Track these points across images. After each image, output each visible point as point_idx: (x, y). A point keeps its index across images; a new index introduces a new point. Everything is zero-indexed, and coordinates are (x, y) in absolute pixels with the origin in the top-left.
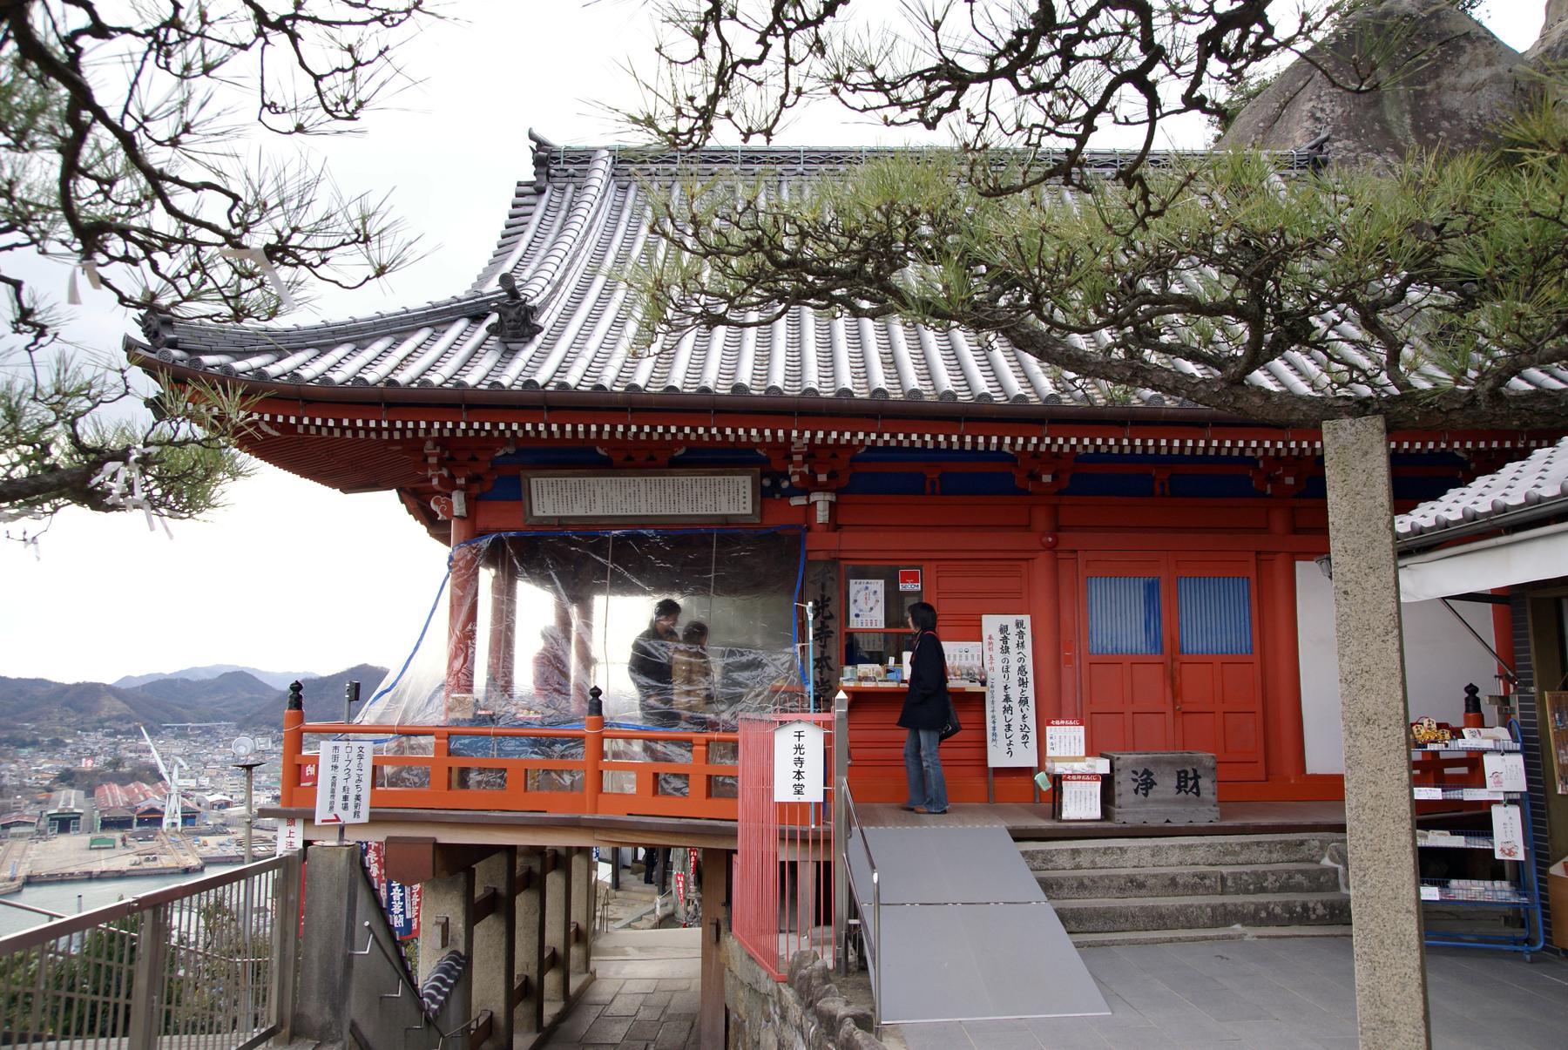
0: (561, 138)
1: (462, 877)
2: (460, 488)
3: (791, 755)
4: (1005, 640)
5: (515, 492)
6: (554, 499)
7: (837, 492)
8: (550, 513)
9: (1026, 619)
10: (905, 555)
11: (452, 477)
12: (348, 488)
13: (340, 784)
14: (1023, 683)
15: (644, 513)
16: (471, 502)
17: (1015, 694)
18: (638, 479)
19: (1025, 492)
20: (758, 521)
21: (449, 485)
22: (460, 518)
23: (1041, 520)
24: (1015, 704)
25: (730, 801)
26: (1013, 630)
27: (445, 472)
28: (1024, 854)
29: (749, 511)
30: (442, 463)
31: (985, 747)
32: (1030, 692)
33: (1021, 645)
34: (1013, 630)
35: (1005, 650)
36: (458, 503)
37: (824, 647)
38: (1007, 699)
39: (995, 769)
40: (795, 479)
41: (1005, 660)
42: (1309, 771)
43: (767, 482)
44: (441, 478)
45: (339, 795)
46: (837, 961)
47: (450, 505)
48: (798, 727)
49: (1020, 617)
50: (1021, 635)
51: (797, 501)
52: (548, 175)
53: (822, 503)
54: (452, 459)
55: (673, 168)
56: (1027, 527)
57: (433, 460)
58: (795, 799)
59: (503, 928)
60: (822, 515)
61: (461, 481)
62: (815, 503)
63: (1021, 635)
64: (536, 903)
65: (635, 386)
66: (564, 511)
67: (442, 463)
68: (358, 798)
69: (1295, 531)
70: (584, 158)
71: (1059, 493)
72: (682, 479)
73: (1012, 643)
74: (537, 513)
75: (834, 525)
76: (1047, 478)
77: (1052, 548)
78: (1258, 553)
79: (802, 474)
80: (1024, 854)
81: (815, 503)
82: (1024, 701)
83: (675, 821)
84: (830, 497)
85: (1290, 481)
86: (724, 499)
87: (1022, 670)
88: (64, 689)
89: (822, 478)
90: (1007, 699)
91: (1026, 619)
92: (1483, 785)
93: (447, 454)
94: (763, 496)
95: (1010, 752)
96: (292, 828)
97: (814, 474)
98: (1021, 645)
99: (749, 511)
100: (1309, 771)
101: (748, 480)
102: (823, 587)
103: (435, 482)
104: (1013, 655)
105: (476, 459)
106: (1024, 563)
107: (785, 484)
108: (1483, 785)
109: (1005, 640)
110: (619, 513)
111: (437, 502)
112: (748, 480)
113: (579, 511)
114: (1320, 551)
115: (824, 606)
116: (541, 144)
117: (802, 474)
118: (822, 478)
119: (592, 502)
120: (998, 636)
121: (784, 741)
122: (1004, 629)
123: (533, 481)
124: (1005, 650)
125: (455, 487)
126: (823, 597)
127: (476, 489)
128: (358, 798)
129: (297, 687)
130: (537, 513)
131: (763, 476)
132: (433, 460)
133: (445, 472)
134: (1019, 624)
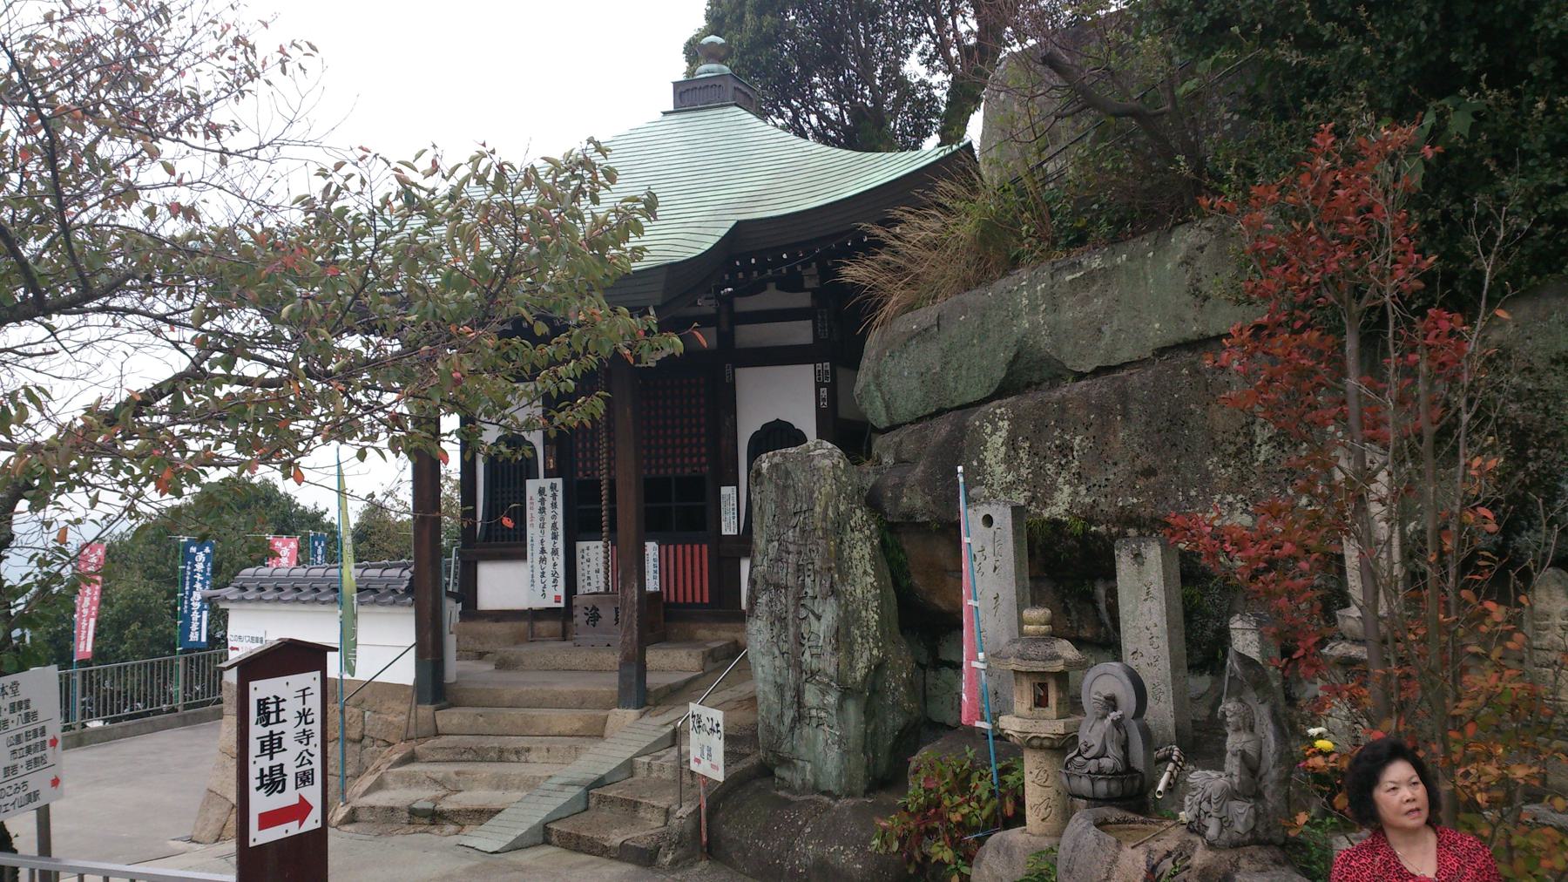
4: (542, 501)
10: (689, 566)
14: (555, 537)
26: (548, 492)
33: (554, 505)
34: (548, 492)
35: (542, 510)
38: (543, 551)
41: (542, 519)
42: (810, 322)
46: (909, 516)
49: (555, 480)
50: (554, 496)
63: (554, 496)
73: (548, 504)
82: (555, 552)
90: (543, 551)
92: (459, 658)
98: (554, 505)
100: (810, 322)
108: (459, 658)
109: (542, 501)
114: (676, 85)
122: (541, 491)
124: (542, 510)
134: (553, 487)
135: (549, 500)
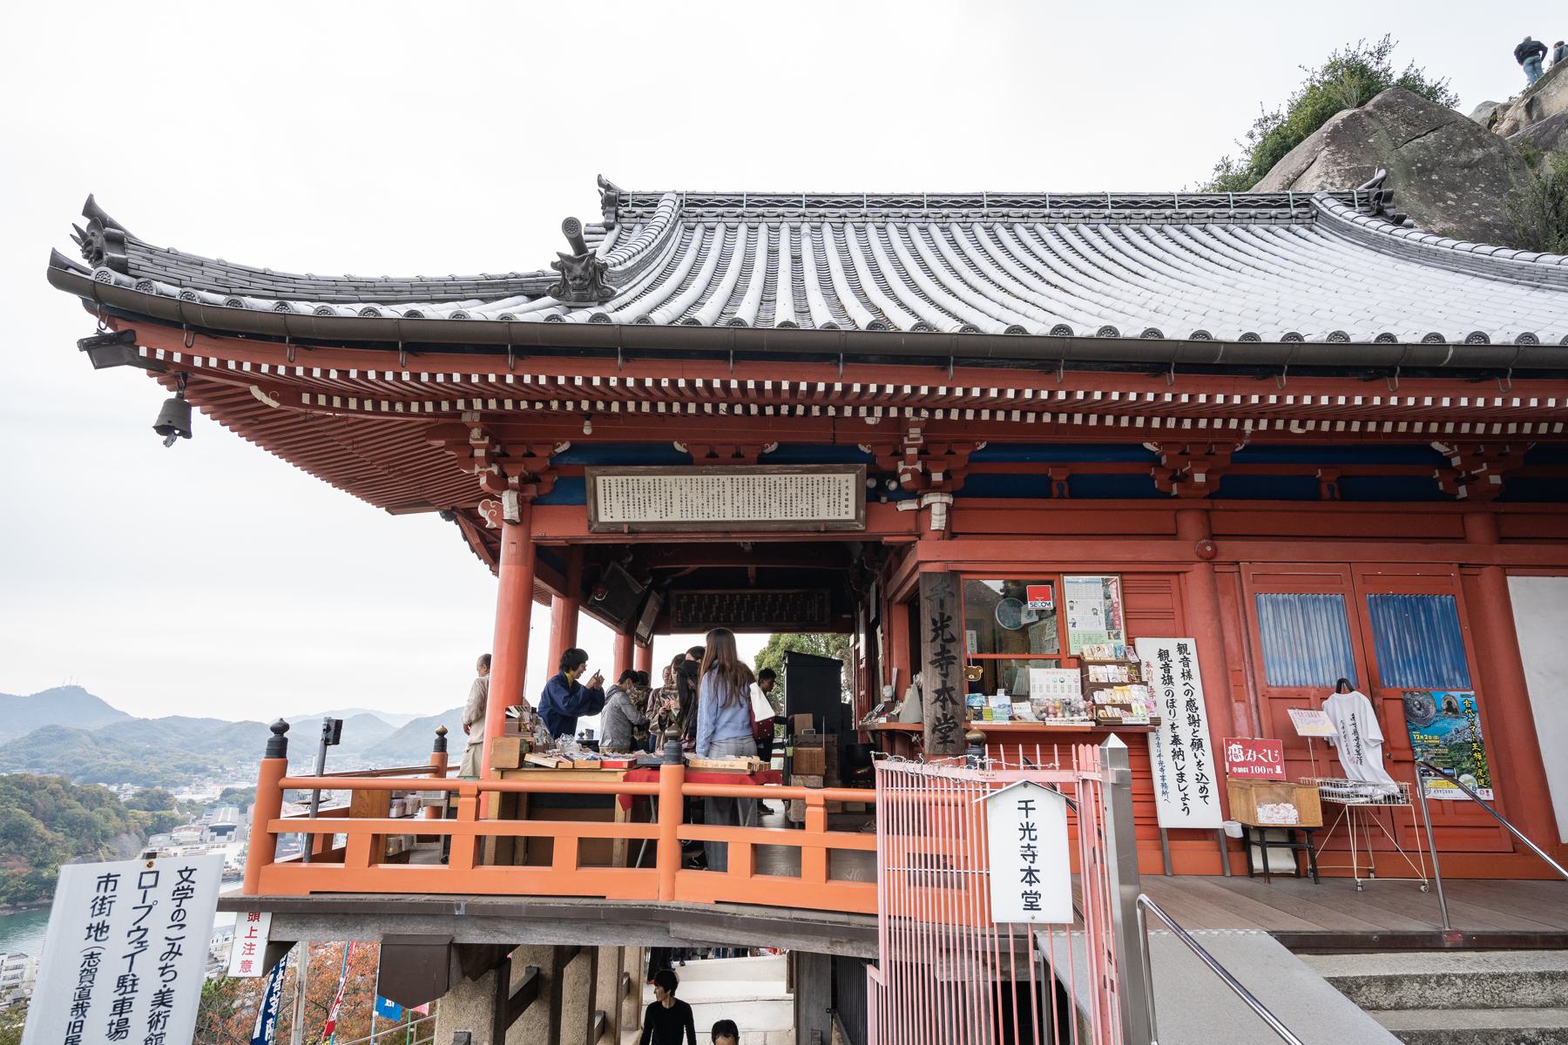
0: (627, 184)
1: (491, 977)
2: (513, 488)
3: (1015, 842)
4: (1166, 667)
5: (577, 492)
6: (628, 502)
7: (955, 494)
8: (618, 518)
9: (1190, 643)
11: (505, 476)
12: (396, 507)
13: (111, 968)
14: (1194, 721)
15: (729, 518)
16: (525, 505)
17: (1185, 733)
18: (723, 478)
19: (1167, 495)
20: (861, 527)
21: (500, 482)
22: (511, 522)
23: (1190, 524)
24: (1186, 746)
25: (868, 886)
26: (1175, 656)
27: (495, 469)
28: (1336, 982)
29: (852, 516)
30: (491, 458)
31: (1152, 801)
32: (1203, 733)
33: (1187, 675)
34: (1175, 656)
35: (1168, 680)
36: (509, 504)
37: (946, 675)
38: (1176, 740)
39: (1170, 831)
40: (906, 478)
43: (872, 483)
44: (490, 475)
45: (104, 995)
47: (500, 509)
48: (1027, 794)
49: (1182, 641)
50: (1185, 661)
51: (906, 506)
52: (617, 215)
53: (937, 506)
54: (504, 454)
55: (739, 210)
56: (1173, 536)
57: (480, 453)
58: (1026, 917)
59: (546, 1020)
60: (937, 521)
61: (514, 480)
62: (929, 507)
63: (1185, 661)
64: (587, 972)
65: (740, 322)
66: (635, 516)
67: (491, 458)
68: (163, 999)
69: (1503, 540)
70: (649, 202)
71: (1211, 496)
72: (774, 477)
74: (603, 518)
75: (950, 533)
76: (1200, 478)
77: (1210, 559)
78: (1461, 566)
79: (914, 473)
80: (1336, 982)
81: (929, 507)
82: (1197, 744)
83: (786, 914)
84: (948, 499)
85: (1495, 479)
86: (823, 501)
87: (1191, 704)
88: (229, 727)
89: (937, 477)
90: (1176, 740)
91: (1190, 643)
93: (498, 449)
94: (874, 495)
95: (1186, 809)
96: (255, 924)
97: (926, 474)
99: (852, 516)
101: (852, 477)
102: (942, 604)
103: (483, 481)
104: (1178, 686)
105: (533, 455)
106: (1173, 578)
107: (893, 485)
109: (1166, 667)
110: (700, 519)
111: (486, 507)
112: (852, 477)
113: (652, 516)
115: (944, 627)
116: (608, 187)
117: (914, 473)
118: (937, 477)
119: (669, 505)
120: (1157, 664)
121: (1003, 819)
122: (1163, 654)
123: (600, 479)
124: (1168, 680)
125: (506, 487)
126: (942, 615)
127: (532, 491)
128: (163, 999)
129: (281, 729)
130: (603, 518)
131: (869, 476)
132: (480, 453)
133: (495, 469)
134: (1182, 648)
135: (1176, 669)
